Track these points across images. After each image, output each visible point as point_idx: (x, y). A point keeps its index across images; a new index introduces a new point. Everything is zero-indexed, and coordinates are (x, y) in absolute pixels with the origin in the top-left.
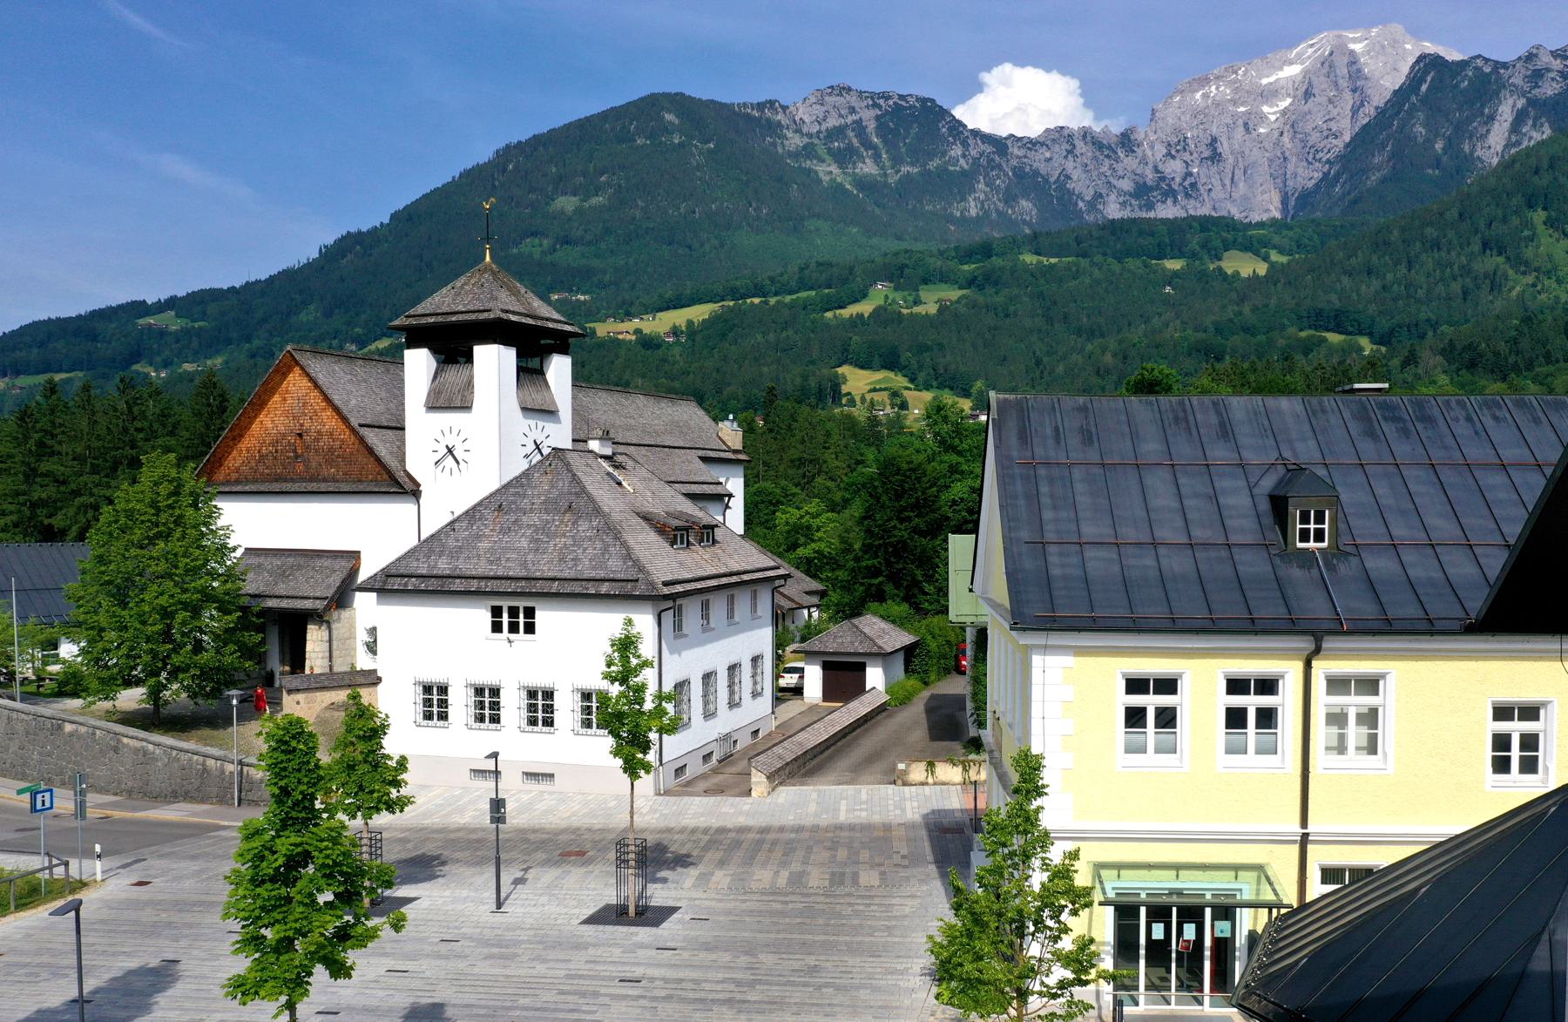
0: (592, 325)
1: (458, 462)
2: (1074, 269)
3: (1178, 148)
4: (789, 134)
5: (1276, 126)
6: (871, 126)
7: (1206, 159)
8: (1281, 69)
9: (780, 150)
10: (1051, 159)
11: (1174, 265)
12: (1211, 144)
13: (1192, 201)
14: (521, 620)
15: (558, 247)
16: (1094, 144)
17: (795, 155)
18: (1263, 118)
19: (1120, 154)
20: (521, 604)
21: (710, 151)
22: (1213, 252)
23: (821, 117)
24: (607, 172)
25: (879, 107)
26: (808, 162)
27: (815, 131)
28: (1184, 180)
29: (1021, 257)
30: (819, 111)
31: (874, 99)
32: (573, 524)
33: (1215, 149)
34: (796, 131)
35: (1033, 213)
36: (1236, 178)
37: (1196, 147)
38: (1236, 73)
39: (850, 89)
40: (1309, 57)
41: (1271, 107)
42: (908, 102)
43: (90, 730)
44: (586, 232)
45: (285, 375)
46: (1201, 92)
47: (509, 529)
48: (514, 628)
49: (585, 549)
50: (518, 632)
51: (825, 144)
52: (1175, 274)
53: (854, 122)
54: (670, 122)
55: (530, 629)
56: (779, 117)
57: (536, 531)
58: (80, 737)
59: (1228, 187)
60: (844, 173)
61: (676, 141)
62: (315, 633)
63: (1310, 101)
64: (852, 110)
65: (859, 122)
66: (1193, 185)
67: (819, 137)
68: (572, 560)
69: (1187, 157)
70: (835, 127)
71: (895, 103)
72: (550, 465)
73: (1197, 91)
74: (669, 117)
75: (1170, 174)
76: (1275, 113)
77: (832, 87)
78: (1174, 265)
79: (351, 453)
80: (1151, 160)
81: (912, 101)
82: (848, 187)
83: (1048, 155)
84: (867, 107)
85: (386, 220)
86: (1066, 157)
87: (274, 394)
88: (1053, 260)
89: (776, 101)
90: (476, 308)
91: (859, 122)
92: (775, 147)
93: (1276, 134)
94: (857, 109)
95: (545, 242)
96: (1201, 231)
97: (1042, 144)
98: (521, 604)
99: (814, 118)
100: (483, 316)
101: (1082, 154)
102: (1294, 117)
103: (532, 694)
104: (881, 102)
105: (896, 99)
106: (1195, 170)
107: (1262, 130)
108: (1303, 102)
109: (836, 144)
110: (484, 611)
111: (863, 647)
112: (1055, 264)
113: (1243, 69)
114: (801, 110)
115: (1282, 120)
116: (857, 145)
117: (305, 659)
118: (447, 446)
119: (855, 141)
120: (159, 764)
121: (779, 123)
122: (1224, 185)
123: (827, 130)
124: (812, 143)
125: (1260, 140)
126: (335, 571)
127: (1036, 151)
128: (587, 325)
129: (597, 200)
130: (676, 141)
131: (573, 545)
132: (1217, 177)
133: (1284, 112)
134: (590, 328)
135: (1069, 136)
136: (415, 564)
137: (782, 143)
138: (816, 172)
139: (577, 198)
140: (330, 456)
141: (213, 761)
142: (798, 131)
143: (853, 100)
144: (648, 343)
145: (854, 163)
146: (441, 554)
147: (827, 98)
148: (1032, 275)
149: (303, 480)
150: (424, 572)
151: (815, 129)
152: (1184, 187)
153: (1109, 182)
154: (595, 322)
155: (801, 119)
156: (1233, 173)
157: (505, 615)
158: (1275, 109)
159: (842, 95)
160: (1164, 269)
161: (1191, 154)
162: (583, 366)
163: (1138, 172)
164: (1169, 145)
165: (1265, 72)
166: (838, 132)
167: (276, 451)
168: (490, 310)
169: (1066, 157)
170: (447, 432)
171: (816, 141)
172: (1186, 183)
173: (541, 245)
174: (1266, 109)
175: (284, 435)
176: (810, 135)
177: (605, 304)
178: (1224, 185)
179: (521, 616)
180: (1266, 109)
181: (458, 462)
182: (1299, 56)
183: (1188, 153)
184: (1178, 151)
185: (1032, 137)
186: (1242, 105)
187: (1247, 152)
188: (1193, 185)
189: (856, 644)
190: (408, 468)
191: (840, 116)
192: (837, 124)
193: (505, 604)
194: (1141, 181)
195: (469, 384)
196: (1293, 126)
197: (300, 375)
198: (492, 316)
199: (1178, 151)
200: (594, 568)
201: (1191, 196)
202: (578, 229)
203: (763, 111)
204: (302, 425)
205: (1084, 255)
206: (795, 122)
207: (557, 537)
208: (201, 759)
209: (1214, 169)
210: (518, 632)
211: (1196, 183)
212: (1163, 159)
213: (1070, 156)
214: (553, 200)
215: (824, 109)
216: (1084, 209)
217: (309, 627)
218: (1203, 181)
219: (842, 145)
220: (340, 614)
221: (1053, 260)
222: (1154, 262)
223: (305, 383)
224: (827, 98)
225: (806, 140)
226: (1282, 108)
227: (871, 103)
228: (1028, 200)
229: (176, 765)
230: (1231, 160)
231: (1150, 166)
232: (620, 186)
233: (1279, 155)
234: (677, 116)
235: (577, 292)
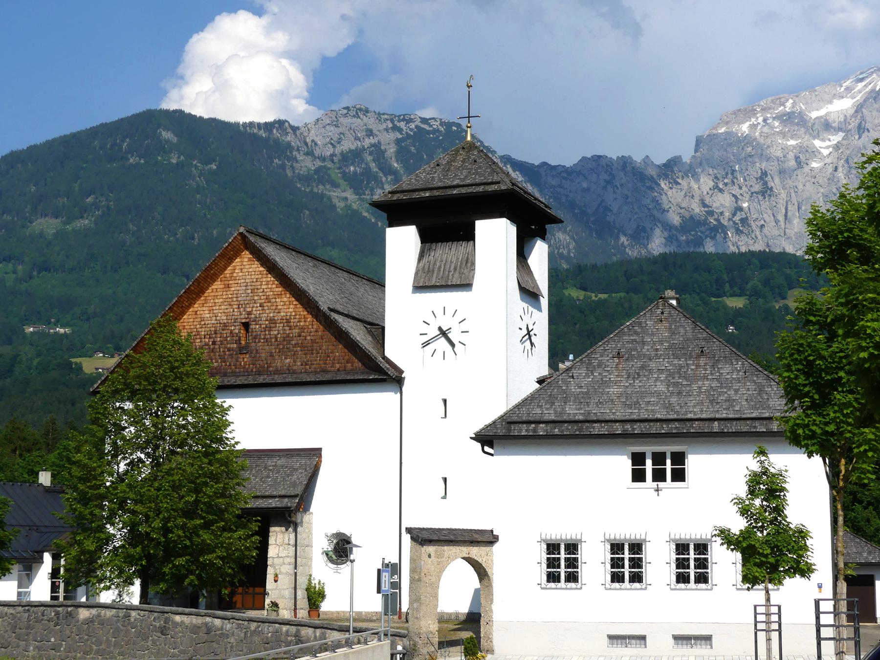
0: (78, 360)
1: (453, 345)
2: (627, 305)
3: (726, 181)
4: (300, 157)
5: (828, 160)
6: (391, 150)
7: (757, 193)
8: (830, 102)
9: (289, 173)
10: (588, 189)
11: (736, 303)
12: (761, 178)
13: (743, 238)
14: (669, 466)
15: (35, 273)
16: (634, 174)
17: (307, 179)
18: (814, 153)
19: (663, 185)
21: (212, 172)
22: (777, 290)
23: (335, 139)
24: (94, 193)
25: (400, 130)
26: (321, 187)
27: (328, 154)
28: (734, 215)
29: (566, 292)
30: (333, 132)
31: (395, 121)
32: (713, 367)
33: (766, 183)
34: (307, 154)
35: (571, 247)
36: (789, 214)
37: (745, 180)
38: (783, 105)
39: (367, 111)
40: (860, 92)
41: (823, 140)
42: (431, 126)
43: (122, 613)
44: (68, 257)
45: (231, 260)
46: (747, 124)
47: (638, 374)
48: (659, 476)
49: (736, 391)
50: (664, 480)
51: (339, 168)
52: (738, 312)
53: (372, 145)
54: (168, 141)
55: (679, 476)
56: (289, 139)
57: (671, 374)
58: (103, 622)
59: (782, 223)
60: (360, 199)
61: (174, 161)
62: (280, 536)
63: (864, 136)
64: (370, 133)
65: (377, 146)
66: (744, 221)
67: (333, 161)
68: (726, 401)
69: (736, 190)
70: (351, 151)
71: (417, 127)
72: (662, 313)
73: (743, 122)
74: (166, 135)
75: (718, 208)
76: (828, 147)
77: (348, 108)
78: (736, 303)
79: (313, 341)
80: (697, 193)
81: (436, 125)
82: (365, 214)
83: (585, 185)
84: (387, 130)
86: (605, 188)
87: (214, 281)
88: (603, 296)
89: (287, 121)
90: (473, 182)
91: (377, 146)
92: (284, 170)
93: (830, 169)
94: (375, 131)
95: (20, 268)
96: (762, 268)
97: (579, 173)
98: (668, 448)
99: (328, 140)
100: (495, 187)
101: (622, 185)
102: (848, 152)
104: (402, 125)
105: (418, 123)
106: (745, 205)
107: (814, 165)
108: (857, 137)
109: (352, 168)
110: (625, 457)
111: (874, 558)
112: (605, 300)
113: (791, 101)
114: (313, 132)
115: (835, 154)
116: (375, 170)
117: (266, 566)
118: (440, 329)
119: (373, 165)
120: (232, 640)
121: (289, 144)
122: (777, 221)
123: (342, 153)
124: (325, 167)
125: (813, 175)
126: (296, 470)
127: (572, 181)
128: (73, 360)
129: (84, 223)
130: (174, 161)
131: (721, 387)
132: (770, 212)
133: (837, 147)
134: (76, 363)
135: (607, 165)
136: (538, 411)
137: (292, 166)
138: (329, 198)
139: (59, 220)
140: (284, 345)
141: (310, 631)
142: (310, 153)
143: (371, 122)
145: (372, 190)
146: (566, 401)
147: (342, 120)
148: (581, 312)
149: (249, 373)
150: (553, 417)
151: (328, 151)
152: (734, 222)
153: (652, 216)
154: (80, 356)
155: (313, 141)
156: (786, 209)
157: (649, 462)
158: (828, 143)
159: (359, 117)
160: (725, 307)
161: (740, 188)
162: (73, 404)
163: (683, 205)
164: (716, 178)
165: (814, 105)
166: (355, 155)
167: (214, 343)
168: (498, 183)
169: (605, 188)
170: (439, 313)
171: (329, 165)
172: (737, 218)
173: (15, 272)
174: (817, 143)
176: (323, 159)
177: (90, 338)
178: (777, 221)
179: (668, 462)
180: (817, 143)
181: (453, 345)
182: (848, 89)
183: (736, 187)
184: (726, 184)
185: (568, 165)
186: (792, 138)
187: (800, 187)
188: (744, 221)
189: (865, 555)
190: (388, 353)
191: (357, 138)
192: (353, 147)
193: (650, 449)
194: (687, 215)
195: (469, 263)
196: (847, 161)
197: (250, 260)
198: (503, 187)
199: (726, 184)
200: (755, 408)
201: (742, 232)
202: (58, 255)
203: (271, 132)
204: (249, 313)
205: (636, 291)
206: (306, 144)
207: (699, 380)
208: (293, 629)
209: (765, 204)
210: (664, 480)
211: (747, 218)
212: (710, 192)
213: (609, 187)
214: (31, 222)
215: (338, 130)
216: (626, 243)
217: (272, 529)
218: (754, 217)
219: (358, 169)
220: (302, 517)
221: (603, 296)
222: (713, 299)
223: (257, 267)
224: (342, 120)
225: (318, 163)
226: (835, 142)
227: (390, 125)
228: (565, 232)
229: (256, 639)
230: (783, 195)
231: (697, 199)
232: (108, 208)
233: (834, 190)
234: (176, 135)
235: (56, 325)
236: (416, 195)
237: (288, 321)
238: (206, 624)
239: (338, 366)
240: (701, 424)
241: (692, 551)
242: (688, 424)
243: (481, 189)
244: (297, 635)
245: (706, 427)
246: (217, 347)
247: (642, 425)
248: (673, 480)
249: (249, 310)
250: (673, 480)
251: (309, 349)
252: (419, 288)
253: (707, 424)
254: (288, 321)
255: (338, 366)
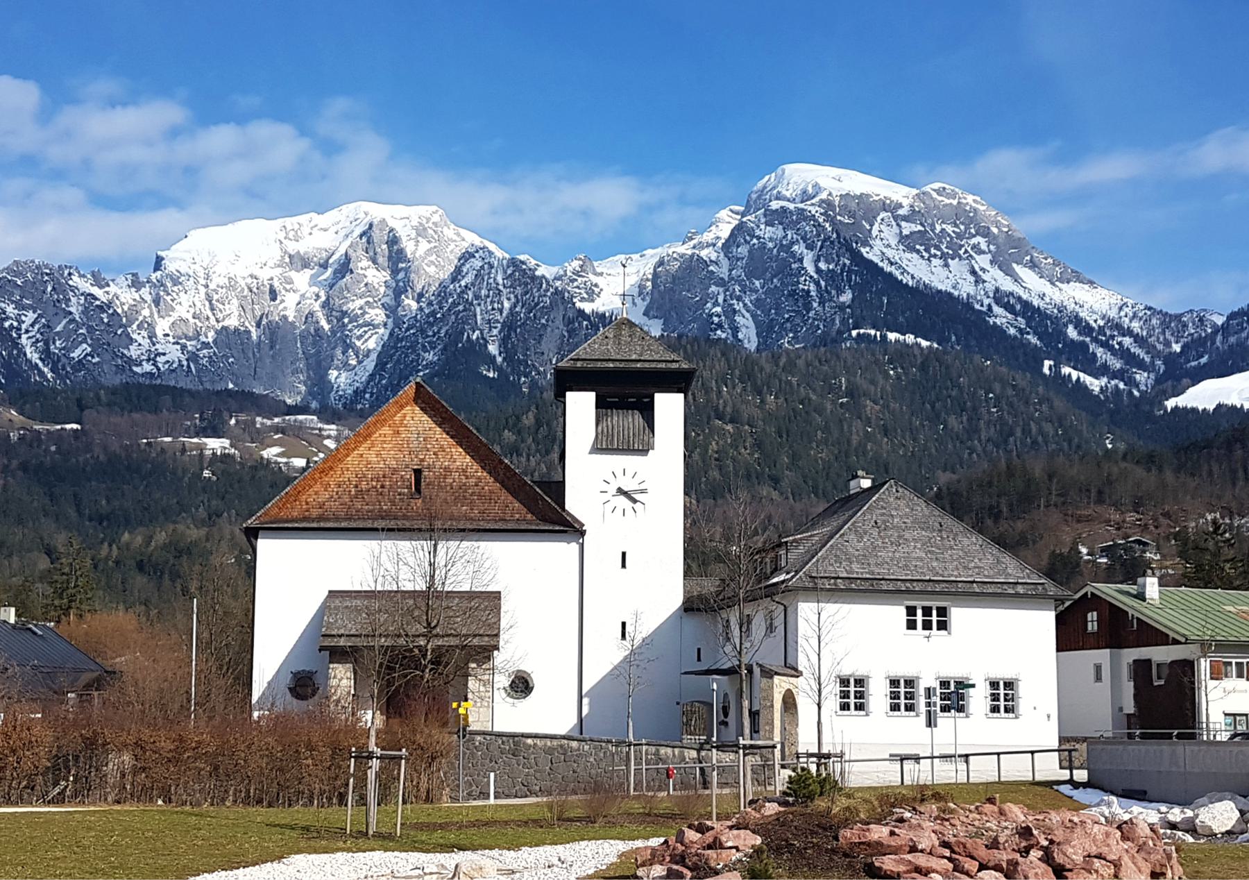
14: (934, 618)
20: (934, 604)
55: (943, 626)
85: (1211, 407)
98: (934, 604)
103: (894, 683)
140: (461, 494)
144: (1080, 386)
157: (919, 612)
167: (382, 487)
170: (619, 473)
175: (395, 471)
193: (919, 603)
204: (422, 460)
236: (599, 365)
237: (464, 471)
238: (561, 746)
239: (517, 516)
240: (964, 585)
241: (902, 697)
242: (954, 584)
243: (663, 365)
244: (657, 753)
245: (967, 587)
246: (386, 490)
247: (920, 584)
248: (939, 629)
249: (422, 457)
250: (939, 629)
251: (490, 498)
252: (597, 449)
253: (968, 585)
254: (464, 471)
255: (517, 516)
